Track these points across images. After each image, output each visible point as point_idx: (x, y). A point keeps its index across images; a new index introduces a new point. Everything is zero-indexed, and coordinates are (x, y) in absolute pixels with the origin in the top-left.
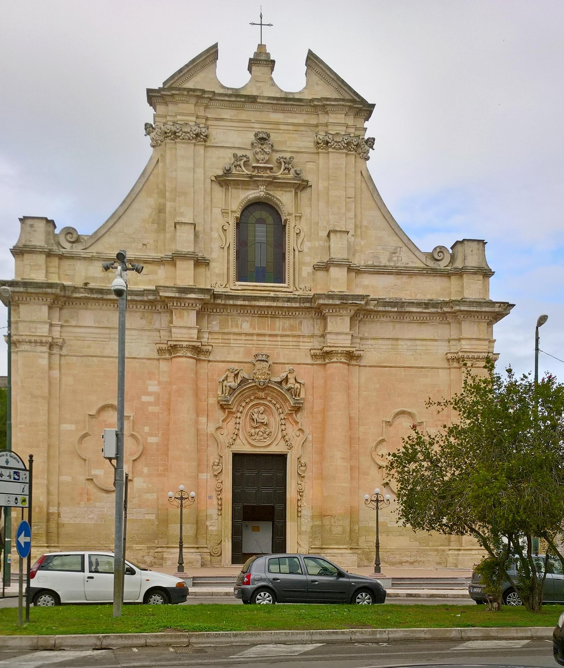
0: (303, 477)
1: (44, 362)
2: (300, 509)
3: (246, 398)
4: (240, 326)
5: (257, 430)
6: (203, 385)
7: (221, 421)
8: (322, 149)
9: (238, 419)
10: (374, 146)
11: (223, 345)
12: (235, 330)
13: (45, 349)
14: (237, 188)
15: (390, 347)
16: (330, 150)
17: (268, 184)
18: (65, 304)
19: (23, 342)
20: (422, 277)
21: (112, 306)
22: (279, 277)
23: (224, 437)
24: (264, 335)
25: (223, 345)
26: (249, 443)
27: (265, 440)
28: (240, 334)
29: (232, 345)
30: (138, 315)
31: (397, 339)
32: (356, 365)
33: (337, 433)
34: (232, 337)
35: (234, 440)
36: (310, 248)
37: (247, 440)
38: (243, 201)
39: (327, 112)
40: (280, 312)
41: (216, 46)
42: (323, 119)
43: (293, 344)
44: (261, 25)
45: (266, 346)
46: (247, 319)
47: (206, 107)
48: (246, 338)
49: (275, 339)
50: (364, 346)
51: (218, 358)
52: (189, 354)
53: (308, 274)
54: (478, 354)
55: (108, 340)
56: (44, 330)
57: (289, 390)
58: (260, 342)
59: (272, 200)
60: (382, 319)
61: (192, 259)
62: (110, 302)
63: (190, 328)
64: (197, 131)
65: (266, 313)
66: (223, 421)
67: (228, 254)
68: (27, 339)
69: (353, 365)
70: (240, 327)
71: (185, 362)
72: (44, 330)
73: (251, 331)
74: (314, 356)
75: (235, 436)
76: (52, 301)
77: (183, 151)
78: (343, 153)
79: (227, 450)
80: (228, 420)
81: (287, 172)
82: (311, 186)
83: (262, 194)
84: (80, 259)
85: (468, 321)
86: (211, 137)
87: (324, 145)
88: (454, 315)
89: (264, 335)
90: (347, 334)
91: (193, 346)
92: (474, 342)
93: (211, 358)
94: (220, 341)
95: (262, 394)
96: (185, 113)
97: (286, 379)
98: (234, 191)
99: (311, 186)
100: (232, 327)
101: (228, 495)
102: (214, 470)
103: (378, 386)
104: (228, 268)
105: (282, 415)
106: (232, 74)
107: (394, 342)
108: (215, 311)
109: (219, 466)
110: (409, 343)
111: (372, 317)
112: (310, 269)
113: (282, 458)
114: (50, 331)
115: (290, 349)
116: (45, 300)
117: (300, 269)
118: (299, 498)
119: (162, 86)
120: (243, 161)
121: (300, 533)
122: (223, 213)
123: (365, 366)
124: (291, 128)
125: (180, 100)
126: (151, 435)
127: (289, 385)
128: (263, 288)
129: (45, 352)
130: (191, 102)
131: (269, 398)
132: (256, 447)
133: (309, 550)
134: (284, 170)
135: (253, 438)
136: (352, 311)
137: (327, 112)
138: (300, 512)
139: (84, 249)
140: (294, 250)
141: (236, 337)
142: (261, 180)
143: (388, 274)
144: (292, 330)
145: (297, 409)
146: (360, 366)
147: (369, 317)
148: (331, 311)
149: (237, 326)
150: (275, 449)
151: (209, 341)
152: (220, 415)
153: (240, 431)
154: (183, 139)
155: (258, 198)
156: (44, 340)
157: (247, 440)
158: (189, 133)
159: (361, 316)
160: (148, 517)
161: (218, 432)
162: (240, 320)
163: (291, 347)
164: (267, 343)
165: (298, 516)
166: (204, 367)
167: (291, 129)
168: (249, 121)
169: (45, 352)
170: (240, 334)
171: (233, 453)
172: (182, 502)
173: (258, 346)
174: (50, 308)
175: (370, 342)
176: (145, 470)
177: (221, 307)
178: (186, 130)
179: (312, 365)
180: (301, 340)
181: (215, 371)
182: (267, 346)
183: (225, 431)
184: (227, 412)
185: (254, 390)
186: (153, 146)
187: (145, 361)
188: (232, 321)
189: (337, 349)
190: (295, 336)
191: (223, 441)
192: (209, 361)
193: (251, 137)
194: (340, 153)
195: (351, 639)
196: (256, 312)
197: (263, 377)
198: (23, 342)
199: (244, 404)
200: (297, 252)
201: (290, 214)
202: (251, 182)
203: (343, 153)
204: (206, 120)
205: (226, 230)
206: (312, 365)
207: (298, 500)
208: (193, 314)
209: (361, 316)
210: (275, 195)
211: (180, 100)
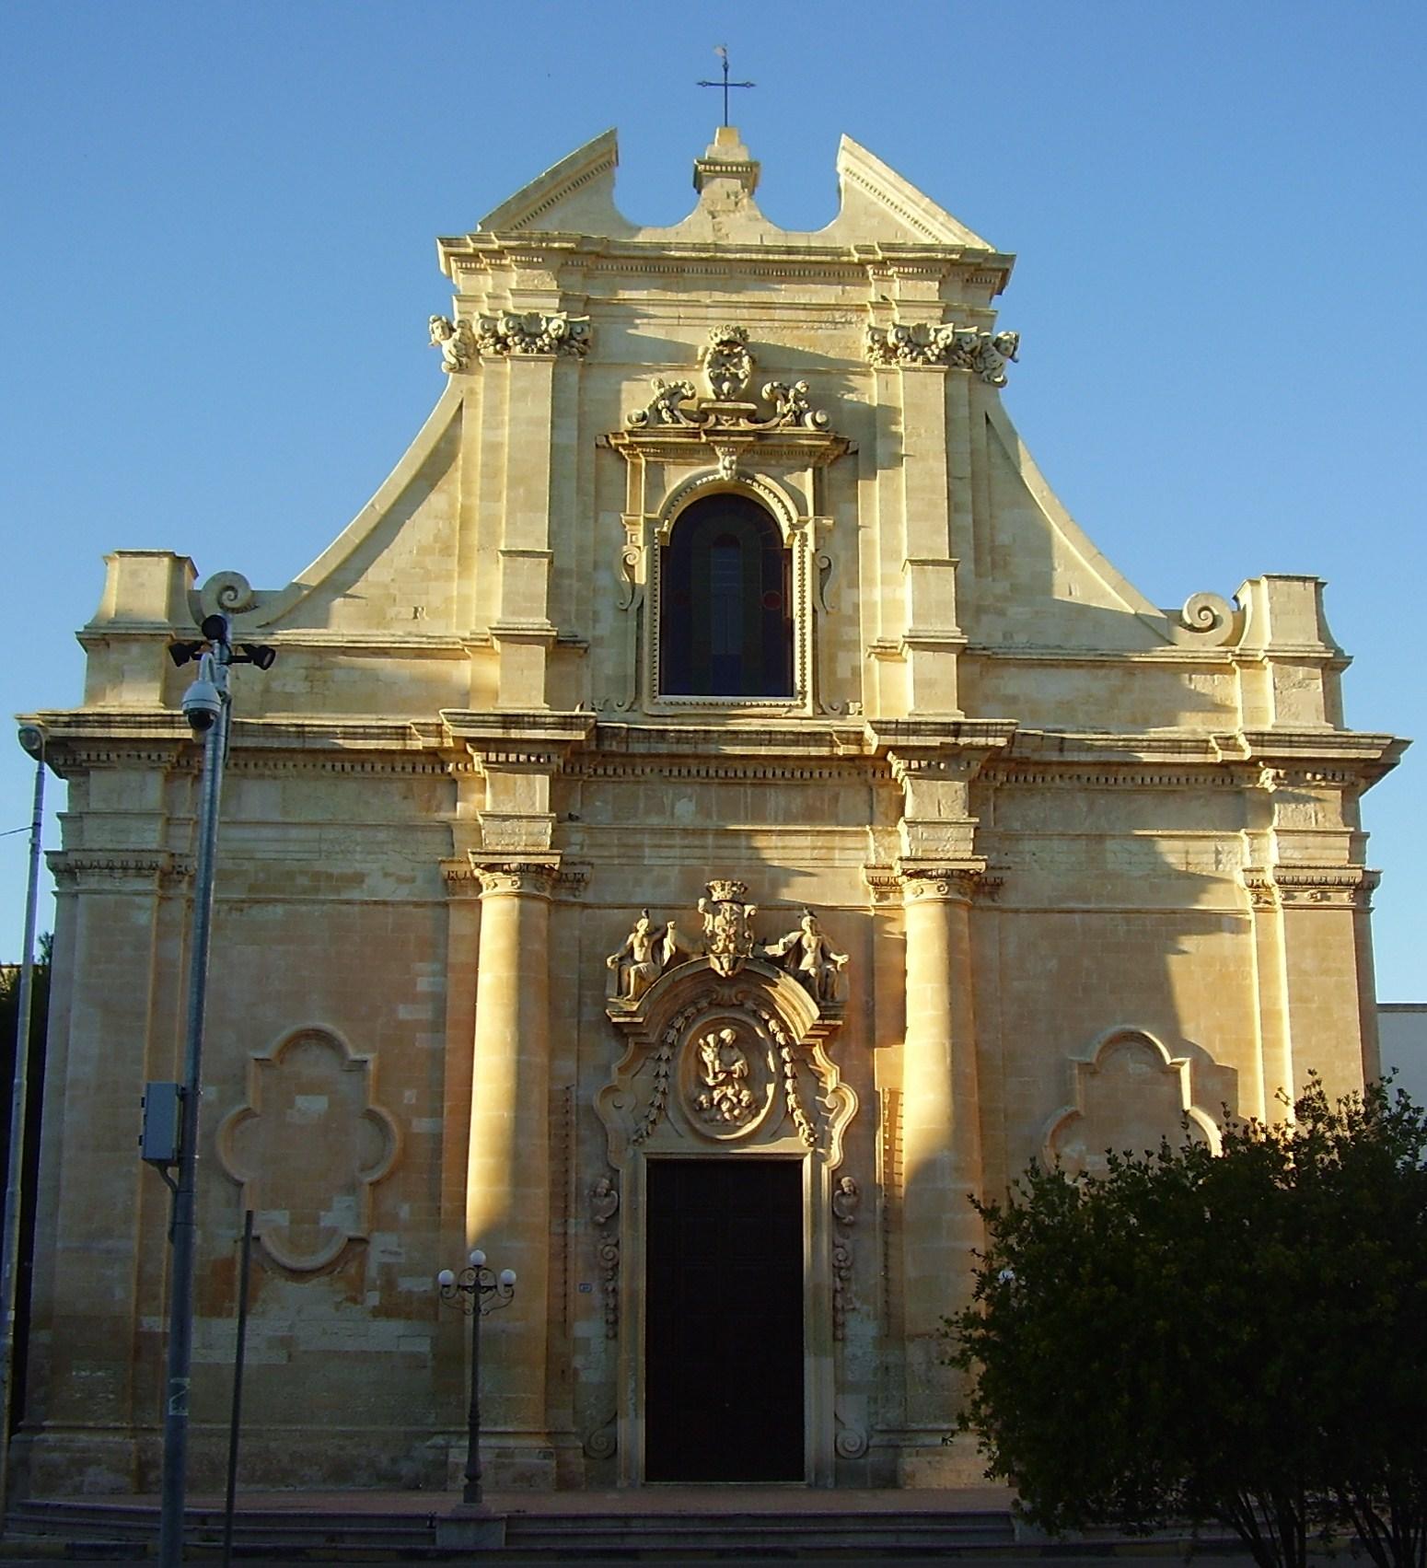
0: (851, 1225)
2: (840, 1318)
3: (685, 1006)
4: (668, 809)
10: (1017, 355)
11: (624, 861)
12: (654, 820)
13: (151, 885)
25: (624, 861)
26: (695, 1131)
28: (669, 832)
32: (990, 909)
34: (647, 840)
35: (654, 1122)
37: (688, 1122)
41: (610, 138)
43: (816, 853)
44: (726, 85)
46: (689, 791)
47: (588, 275)
48: (686, 842)
50: (1009, 858)
62: (321, 758)
65: (740, 774)
67: (640, 626)
68: (102, 858)
69: (981, 909)
72: (150, 837)
73: (700, 822)
75: (654, 1111)
93: (588, 897)
94: (615, 851)
100: (648, 812)
101: (634, 1281)
102: (596, 1211)
104: (639, 661)
108: (600, 771)
114: (166, 837)
116: (154, 757)
118: (839, 1285)
121: (841, 1387)
123: (1017, 911)
124: (802, 315)
129: (146, 894)
131: (749, 1005)
133: (870, 1437)
135: (706, 1115)
136: (973, 763)
138: (843, 1324)
143: (1067, 667)
146: (1003, 911)
149: (661, 811)
153: (670, 1098)
157: (688, 1122)
159: (1002, 777)
160: (406, 1347)
165: (835, 1339)
169: (146, 894)
170: (669, 832)
171: (648, 1161)
172: (477, 1297)
174: (169, 778)
176: (405, 1211)
177: (618, 760)
182: (745, 863)
183: (627, 1100)
184: (631, 1045)
187: (410, 908)
192: (585, 906)
195: (588, 275)
196: (712, 772)
199: (680, 1022)
204: (586, 305)
207: (836, 1291)
209: (1002, 777)
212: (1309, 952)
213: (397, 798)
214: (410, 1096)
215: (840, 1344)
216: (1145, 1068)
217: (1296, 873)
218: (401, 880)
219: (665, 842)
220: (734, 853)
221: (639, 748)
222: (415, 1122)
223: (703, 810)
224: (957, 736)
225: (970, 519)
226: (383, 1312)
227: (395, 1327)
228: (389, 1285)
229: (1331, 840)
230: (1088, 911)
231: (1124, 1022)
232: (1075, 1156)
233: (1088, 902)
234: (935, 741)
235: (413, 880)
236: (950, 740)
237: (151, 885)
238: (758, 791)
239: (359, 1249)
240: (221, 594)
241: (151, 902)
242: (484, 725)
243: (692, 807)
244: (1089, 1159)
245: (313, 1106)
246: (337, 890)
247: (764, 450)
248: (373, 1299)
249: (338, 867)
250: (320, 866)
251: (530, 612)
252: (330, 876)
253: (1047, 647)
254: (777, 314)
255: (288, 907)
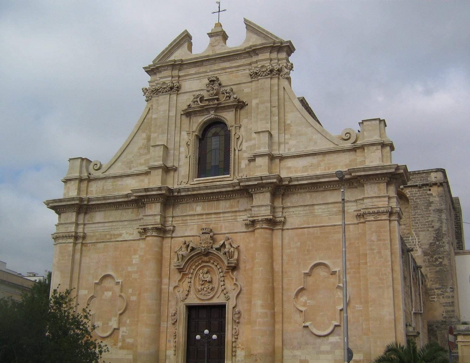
0: (238, 323)
1: (70, 247)
2: (234, 349)
4: (195, 209)
5: (203, 287)
6: (166, 255)
7: (177, 281)
8: (254, 78)
9: (189, 279)
12: (191, 213)
14: (196, 116)
15: (308, 212)
16: (259, 78)
17: (216, 109)
18: (87, 209)
19: (59, 237)
20: (293, 159)
21: (114, 207)
22: (226, 170)
23: (180, 295)
24: (211, 214)
25: (183, 224)
27: (209, 294)
29: (188, 224)
30: (130, 211)
31: (313, 205)
33: (259, 286)
34: (188, 218)
36: (247, 147)
38: (200, 123)
39: (257, 54)
40: (222, 196)
42: (254, 59)
43: (232, 218)
44: (219, 11)
45: (213, 222)
48: (198, 218)
49: (219, 216)
51: (179, 235)
52: (154, 234)
53: (246, 165)
54: (378, 209)
55: (111, 230)
56: (72, 228)
57: (225, 254)
58: (208, 220)
59: (220, 119)
60: (300, 191)
61: (161, 168)
63: (155, 215)
64: (177, 86)
66: (180, 281)
70: (194, 210)
71: (152, 240)
73: (202, 212)
74: (247, 225)
76: (389, 179)
77: (163, 99)
78: (269, 78)
79: (181, 303)
80: (183, 280)
81: (228, 98)
82: (247, 105)
83: (213, 116)
84: (100, 180)
85: (369, 184)
86: (183, 88)
87: (255, 75)
88: (356, 180)
89: (211, 214)
90: (385, 197)
91: (266, 219)
92: (374, 200)
93: (174, 235)
94: (180, 222)
95: (206, 259)
96: (165, 78)
97: (223, 245)
98: (195, 118)
99: (247, 105)
102: (173, 320)
103: (299, 244)
105: (221, 273)
106: (201, 46)
107: (311, 208)
108: (176, 201)
109: (175, 317)
110: (323, 207)
111: (292, 190)
112: (247, 162)
113: (222, 308)
115: (228, 222)
117: (239, 163)
119: (152, 63)
120: (199, 98)
122: (188, 134)
124: (234, 69)
125: (162, 70)
126: (132, 295)
127: (226, 250)
128: (227, 180)
130: (168, 69)
131: (212, 261)
132: (203, 300)
134: (226, 98)
135: (200, 293)
136: (270, 188)
137: (257, 54)
138: (235, 352)
139: (103, 173)
140: (235, 149)
141: (191, 218)
142: (209, 108)
144: (232, 208)
145: (234, 268)
147: (289, 190)
148: (253, 190)
149: (193, 210)
150: (217, 300)
151: (173, 223)
152: (178, 276)
154: (163, 93)
155: (211, 119)
156: (70, 234)
158: (166, 88)
161: (176, 290)
162: (194, 205)
163: (231, 220)
164: (214, 219)
166: (167, 243)
167: (234, 70)
168: (206, 72)
170: (194, 215)
173: (206, 222)
175: (291, 210)
178: (164, 87)
179: (246, 232)
180: (238, 214)
181: (174, 246)
182: (213, 222)
185: (202, 256)
186: (147, 101)
188: (189, 206)
189: (257, 218)
190: (233, 212)
191: (179, 296)
193: (206, 81)
194: (266, 78)
197: (206, 245)
198: (59, 237)
200: (237, 151)
201: (232, 126)
202: (203, 110)
203: (269, 78)
205: (189, 145)
206: (246, 232)
207: (233, 342)
208: (268, 195)
210: (222, 115)
211: (162, 70)
212: (374, 234)
213: (130, 213)
214: (130, 291)
215: (234, 358)
216: (325, 273)
217: (369, 210)
218: (130, 234)
219: (193, 218)
220: (211, 220)
221: (183, 194)
222: (131, 298)
223: (203, 209)
224: (262, 180)
225: (277, 118)
226: (122, 348)
227: (125, 352)
228: (124, 340)
229: (382, 199)
230: (309, 228)
231: (319, 260)
232: (304, 301)
233: (309, 224)
234: (256, 183)
235: (133, 234)
236: (261, 182)
237: (72, 240)
238: (218, 202)
239: (117, 331)
240: (94, 166)
241: (72, 244)
242: (141, 192)
243: (201, 208)
244: (308, 301)
245: (109, 294)
246: (116, 238)
247: (218, 108)
248: (120, 344)
249: (116, 232)
250: (112, 233)
251: (158, 161)
252: (114, 235)
253: (300, 152)
254: (228, 70)
255: (104, 243)
